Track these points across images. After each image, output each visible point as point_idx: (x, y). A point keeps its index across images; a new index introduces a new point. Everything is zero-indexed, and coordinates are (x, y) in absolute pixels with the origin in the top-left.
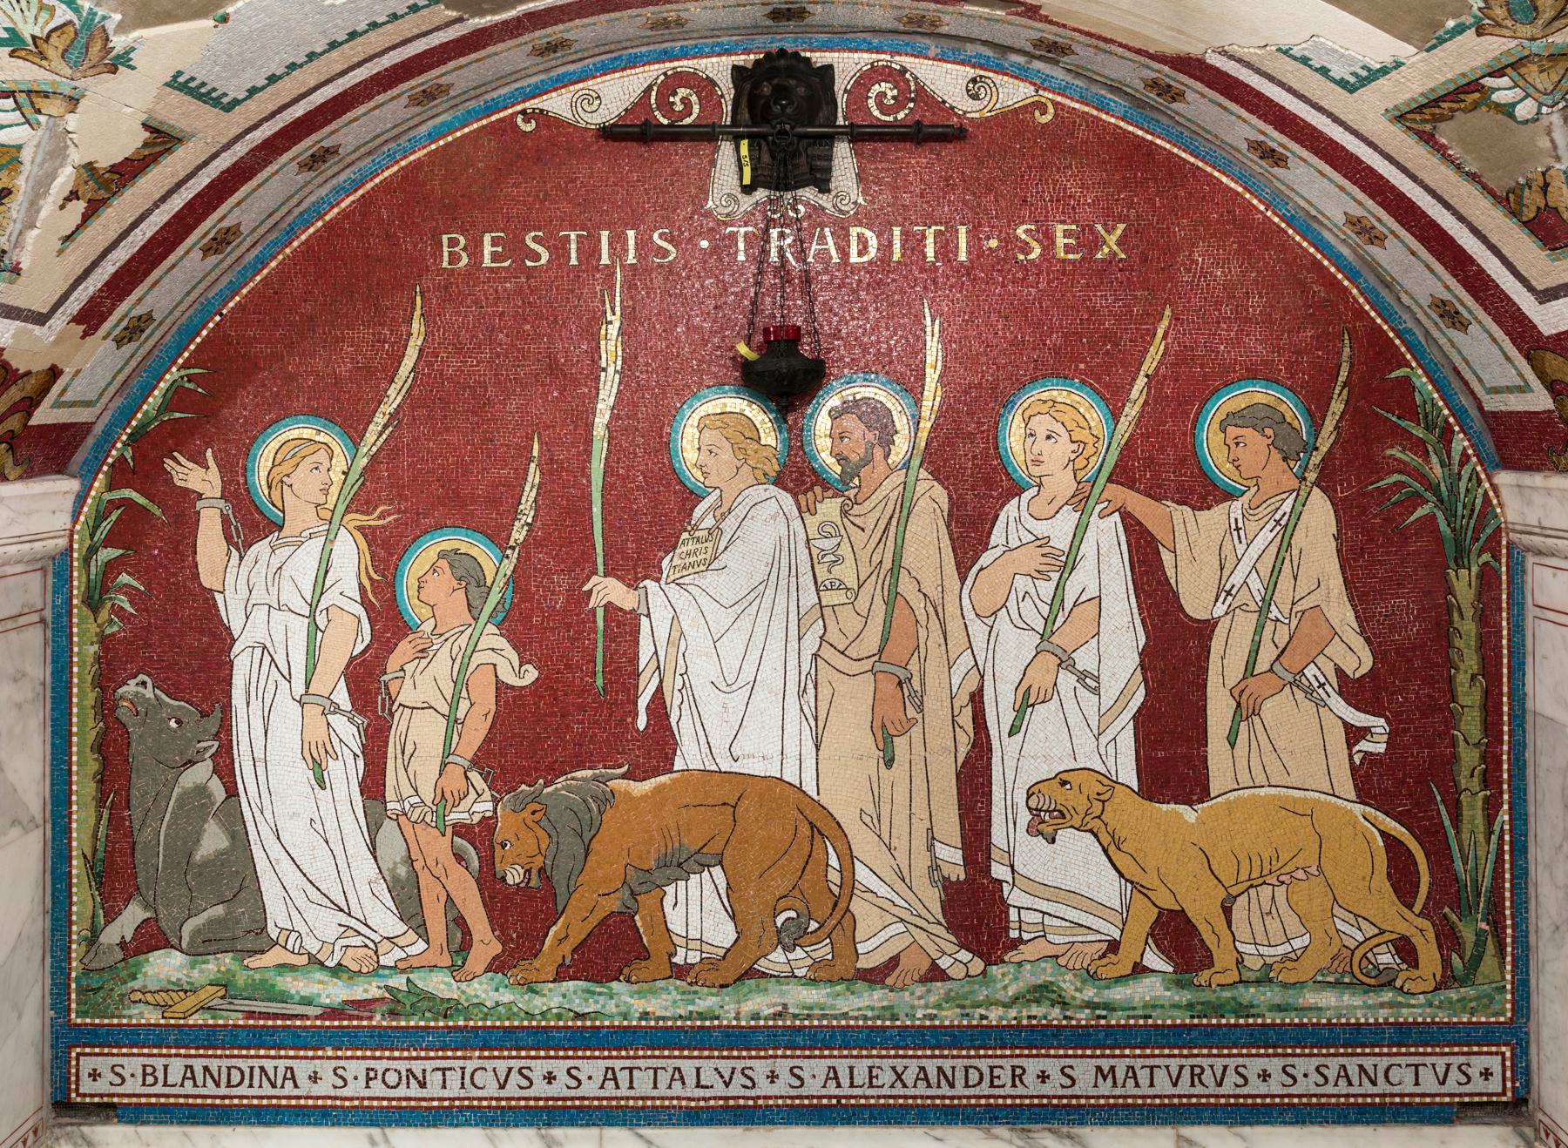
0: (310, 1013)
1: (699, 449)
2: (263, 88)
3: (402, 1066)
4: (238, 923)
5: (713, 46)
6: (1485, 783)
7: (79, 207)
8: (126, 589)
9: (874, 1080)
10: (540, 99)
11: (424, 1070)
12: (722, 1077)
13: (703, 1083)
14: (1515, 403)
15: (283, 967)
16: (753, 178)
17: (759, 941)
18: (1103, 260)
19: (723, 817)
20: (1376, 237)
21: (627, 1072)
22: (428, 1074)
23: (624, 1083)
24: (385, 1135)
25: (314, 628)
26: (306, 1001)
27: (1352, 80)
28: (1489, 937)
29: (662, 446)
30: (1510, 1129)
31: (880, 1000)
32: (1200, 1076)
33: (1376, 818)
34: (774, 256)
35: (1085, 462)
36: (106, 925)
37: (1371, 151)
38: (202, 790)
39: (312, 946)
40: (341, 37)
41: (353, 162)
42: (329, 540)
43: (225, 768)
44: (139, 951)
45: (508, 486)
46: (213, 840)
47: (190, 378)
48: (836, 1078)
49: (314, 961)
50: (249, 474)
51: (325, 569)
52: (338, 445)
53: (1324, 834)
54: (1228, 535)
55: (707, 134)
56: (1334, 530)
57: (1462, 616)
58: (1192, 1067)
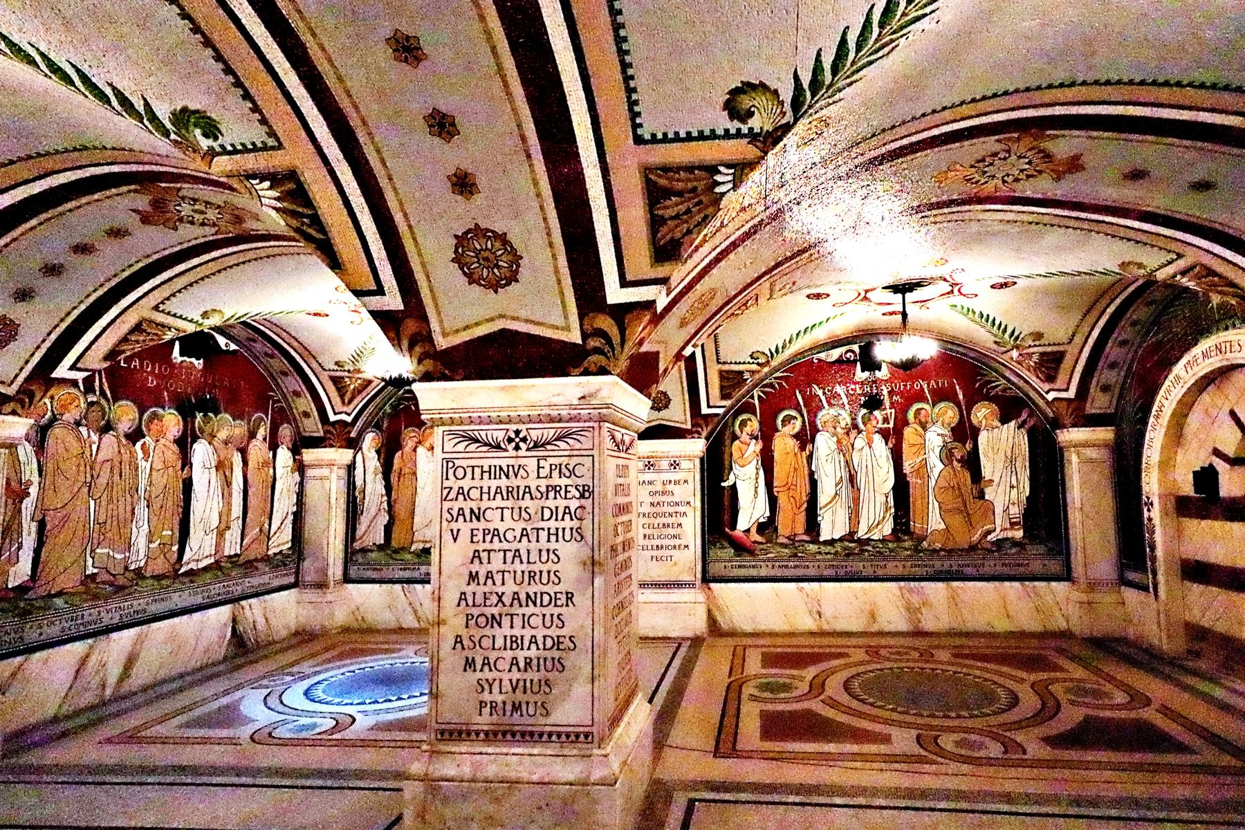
4: (623, 509)
7: (299, 638)
11: (520, 541)
13: (629, 277)
16: (657, 215)
19: (353, 572)
20: (961, 511)
21: (486, 553)
23: (499, 582)
30: (241, 708)
32: (571, 599)
34: (1062, 662)
35: (418, 694)
37: (606, 212)
44: (287, 179)
45: (408, 399)
52: (753, 418)
54: (568, 447)
58: (530, 572)
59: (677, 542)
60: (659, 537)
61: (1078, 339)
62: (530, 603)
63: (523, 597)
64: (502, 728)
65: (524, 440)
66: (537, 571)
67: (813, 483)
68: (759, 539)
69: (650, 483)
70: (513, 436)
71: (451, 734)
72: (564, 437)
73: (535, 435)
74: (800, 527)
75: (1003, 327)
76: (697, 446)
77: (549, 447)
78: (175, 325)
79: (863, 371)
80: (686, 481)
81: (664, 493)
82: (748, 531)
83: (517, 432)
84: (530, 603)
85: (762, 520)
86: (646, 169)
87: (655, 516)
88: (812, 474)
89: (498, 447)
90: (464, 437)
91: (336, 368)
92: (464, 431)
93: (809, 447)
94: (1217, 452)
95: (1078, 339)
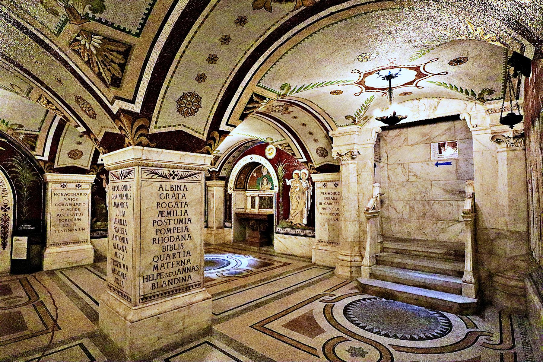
0: (248, 52)
1: (507, 164)
2: (270, 68)
5: (154, 286)
6: (532, 108)
12: (254, 325)
13: (229, 123)
14: (208, 176)
18: (485, 93)
24: (520, 113)
27: (503, 96)
29: (122, 52)
33: (234, 204)
36: (35, 144)
38: (103, 206)
40: (283, 57)
43: (105, 204)
46: (104, 211)
47: (257, 103)
55: (512, 111)
61: (45, 126)
62: (183, 239)
63: (180, 237)
64: (175, 289)
65: (176, 175)
66: (181, 227)
70: (172, 173)
71: (176, 291)
72: (194, 174)
73: (181, 173)
75: (126, 266)
76: (91, 178)
77: (186, 179)
78: (93, 75)
79: (289, 180)
83: (174, 172)
84: (183, 239)
86: (254, 93)
90: (151, 172)
92: (151, 169)
95: (45, 126)
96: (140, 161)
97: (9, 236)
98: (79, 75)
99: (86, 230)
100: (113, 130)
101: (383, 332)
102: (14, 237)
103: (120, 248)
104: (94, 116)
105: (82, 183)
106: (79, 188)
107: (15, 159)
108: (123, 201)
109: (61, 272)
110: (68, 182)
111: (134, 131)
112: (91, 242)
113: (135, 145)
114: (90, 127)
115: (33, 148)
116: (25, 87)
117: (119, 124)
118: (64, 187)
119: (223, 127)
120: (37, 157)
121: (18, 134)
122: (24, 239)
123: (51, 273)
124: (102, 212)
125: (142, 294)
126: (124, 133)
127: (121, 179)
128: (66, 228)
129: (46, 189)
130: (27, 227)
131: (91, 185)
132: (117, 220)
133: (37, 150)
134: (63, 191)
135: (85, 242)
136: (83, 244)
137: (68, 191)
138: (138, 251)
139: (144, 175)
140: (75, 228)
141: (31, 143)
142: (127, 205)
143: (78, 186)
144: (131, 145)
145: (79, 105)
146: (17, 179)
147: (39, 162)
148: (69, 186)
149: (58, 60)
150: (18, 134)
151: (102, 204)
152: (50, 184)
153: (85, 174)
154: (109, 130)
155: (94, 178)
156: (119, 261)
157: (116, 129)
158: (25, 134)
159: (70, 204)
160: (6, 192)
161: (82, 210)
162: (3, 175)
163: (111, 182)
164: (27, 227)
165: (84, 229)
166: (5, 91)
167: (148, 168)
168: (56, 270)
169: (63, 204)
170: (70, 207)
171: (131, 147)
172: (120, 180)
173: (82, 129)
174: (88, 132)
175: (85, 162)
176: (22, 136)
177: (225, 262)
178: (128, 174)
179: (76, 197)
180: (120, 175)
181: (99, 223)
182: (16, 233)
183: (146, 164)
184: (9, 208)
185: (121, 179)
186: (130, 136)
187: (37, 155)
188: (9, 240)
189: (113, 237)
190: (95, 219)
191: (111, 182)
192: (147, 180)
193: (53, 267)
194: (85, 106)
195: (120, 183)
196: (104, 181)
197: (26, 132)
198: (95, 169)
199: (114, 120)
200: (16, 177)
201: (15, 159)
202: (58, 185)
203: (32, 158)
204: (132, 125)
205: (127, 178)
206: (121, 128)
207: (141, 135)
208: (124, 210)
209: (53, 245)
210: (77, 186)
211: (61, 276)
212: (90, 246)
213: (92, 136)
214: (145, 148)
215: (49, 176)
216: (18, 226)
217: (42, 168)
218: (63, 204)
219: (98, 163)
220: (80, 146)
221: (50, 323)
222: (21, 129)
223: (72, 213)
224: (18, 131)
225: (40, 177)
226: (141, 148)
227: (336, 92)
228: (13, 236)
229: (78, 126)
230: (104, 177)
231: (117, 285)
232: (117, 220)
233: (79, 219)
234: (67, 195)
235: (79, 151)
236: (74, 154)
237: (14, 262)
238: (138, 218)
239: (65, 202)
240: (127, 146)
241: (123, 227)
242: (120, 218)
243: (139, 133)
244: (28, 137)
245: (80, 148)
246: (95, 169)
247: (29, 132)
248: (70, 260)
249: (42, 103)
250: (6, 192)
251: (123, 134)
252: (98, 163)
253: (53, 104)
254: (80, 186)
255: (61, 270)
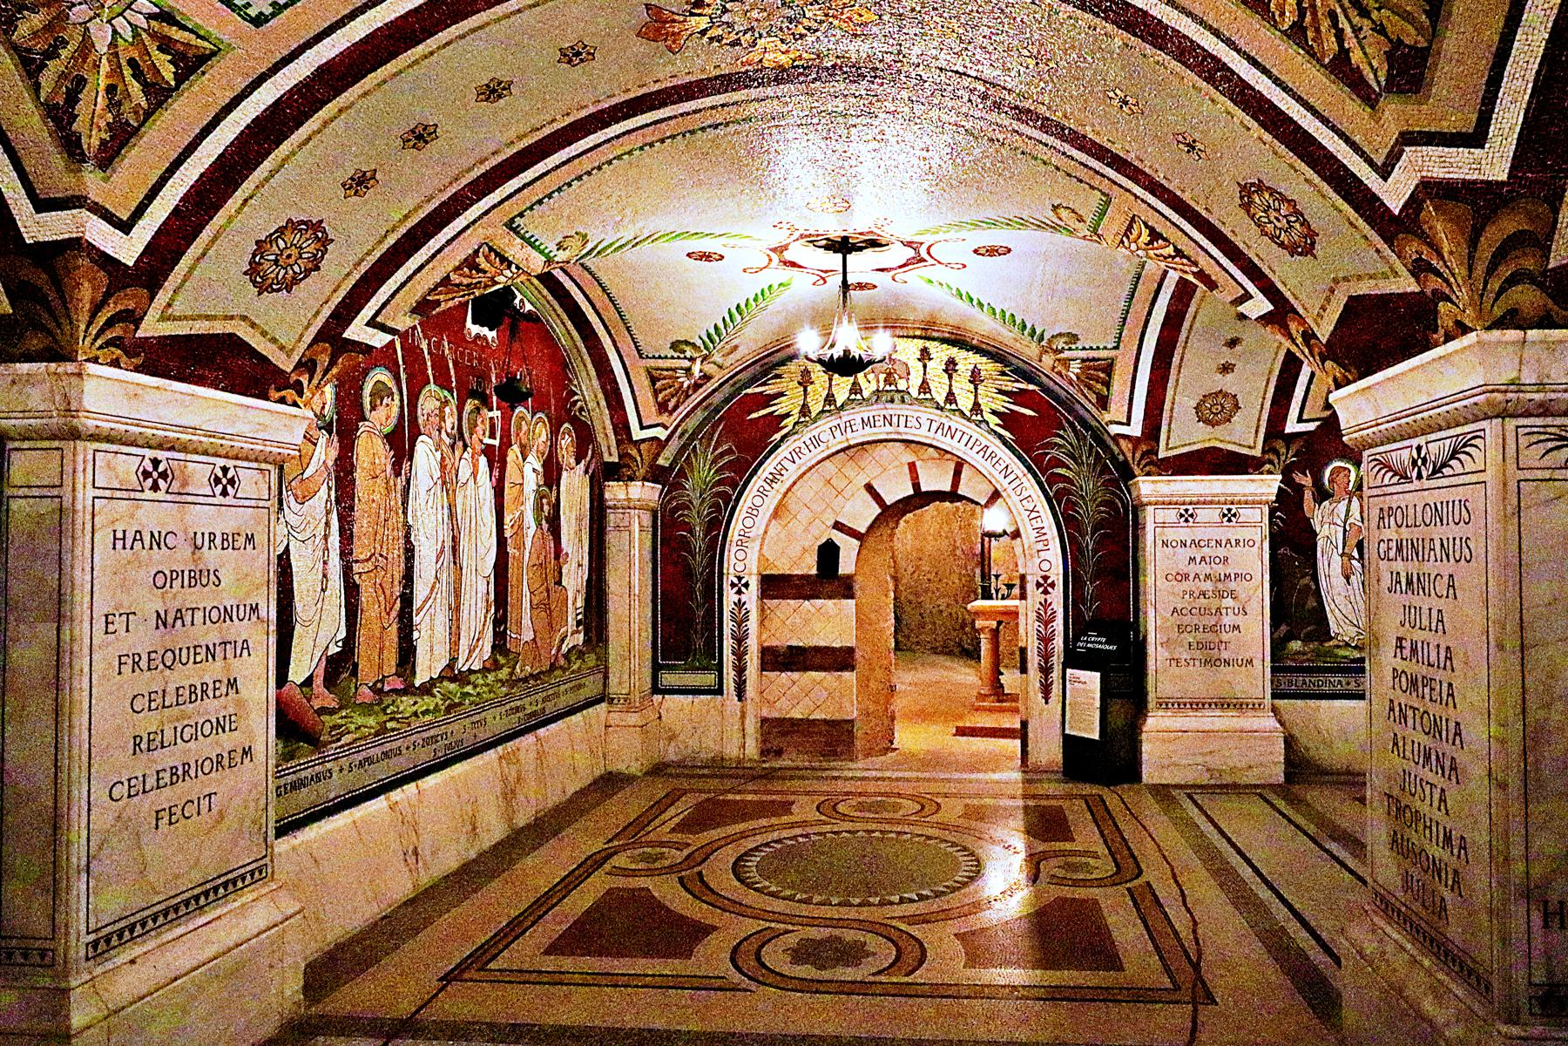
3: (734, 549)
8: (1279, 517)
9: (110, 626)
10: (463, 628)
15: (1338, 647)
17: (972, 134)
22: (1445, 594)
25: (1345, 531)
26: (1345, 657)
28: (104, 60)
31: (1303, 939)
35: (896, 898)
38: (1307, 586)
39: (1347, 639)
41: (309, 138)
42: (1350, 502)
43: (1315, 578)
46: (1312, 603)
48: (141, 540)
49: (1347, 645)
50: (67, 543)
51: (1348, 511)
53: (241, 311)
56: (416, 635)
57: (1373, 911)
59: (227, 741)
60: (179, 735)
67: (409, 552)
68: (331, 701)
69: (157, 541)
74: (390, 666)
75: (1008, 315)
76: (1268, 485)
80: (250, 539)
81: (197, 577)
82: (308, 682)
85: (333, 650)
87: (170, 658)
88: (408, 529)
89: (1404, 477)
91: (671, 353)
93: (406, 466)
94: (838, 526)
96: (1510, 395)
97: (1055, 666)
98: (1260, 97)
99: (1257, 663)
100: (1381, 283)
101: (835, 901)
102: (1069, 671)
103: (1427, 758)
104: (1305, 247)
105: (1239, 502)
106: (1229, 520)
107: (1058, 440)
108: (1430, 567)
109: (1190, 796)
110: (1198, 503)
111: (1480, 269)
112: (1274, 709)
113: (1489, 328)
114: (1288, 295)
115: (1103, 402)
116: (1089, 203)
117: (1412, 248)
118: (1187, 521)
119: (357, 331)
120: (1114, 429)
121: (1066, 363)
122: (1092, 679)
123: (1163, 792)
124: (1303, 606)
125: (1539, 977)
126: (1434, 283)
127: (1419, 477)
128: (1198, 654)
129: (1138, 526)
130: (1096, 642)
131: (1266, 510)
132: (1407, 644)
133: (1113, 407)
134: (1184, 534)
135: (1257, 707)
136: (1251, 713)
137: (1199, 534)
138: (1515, 783)
139: (1532, 456)
140: (1225, 655)
141: (1099, 386)
142: (1451, 586)
143: (1229, 516)
144: (1464, 329)
145: (1252, 216)
146: (1068, 500)
147: (1118, 444)
148: (1203, 514)
149: (1188, 67)
150: (1066, 363)
151: (1303, 577)
152: (1150, 509)
153: (1247, 473)
154: (1364, 288)
155: (1277, 484)
156: (1424, 808)
157: (1396, 274)
158: (1083, 361)
159: (1208, 577)
160: (1043, 538)
161: (1243, 596)
162: (1037, 487)
163: (1375, 492)
164: (1096, 642)
165: (1250, 662)
166: (1039, 233)
167: (1549, 420)
168: (1177, 786)
169: (1186, 577)
170: (1208, 586)
171: (1471, 338)
172: (1416, 484)
173: (1259, 305)
174: (1281, 314)
175: (1244, 434)
176: (1075, 367)
177: (872, 941)
178: (1452, 457)
179: (1221, 552)
180: (1414, 463)
181: (1296, 645)
182: (1074, 659)
183: (1541, 404)
184: (746, 585)
185: (1419, 477)
186: (1463, 295)
187: (1112, 422)
188: (1056, 675)
189: (1392, 709)
190: (1284, 628)
191: (1375, 492)
192: (1547, 474)
193: (1168, 778)
194: (1273, 214)
195: (1413, 497)
196: (1308, 495)
197: (1083, 354)
198: (1278, 455)
199: (1389, 240)
200: (1066, 492)
201: (1058, 440)
202: (1171, 515)
203: (1099, 435)
204: (1473, 243)
205: (1446, 471)
206: (1419, 269)
207: (1512, 281)
208: (1437, 604)
209: (1164, 704)
210: (1224, 515)
211: (1188, 804)
212: (1270, 722)
213: (1293, 326)
214: (1533, 334)
215: (1147, 487)
216: (1076, 639)
217: (1126, 460)
218: (1186, 577)
219: (1288, 430)
220: (1229, 376)
221: (1186, 976)
222: (1073, 347)
223: (1214, 603)
224: (1067, 354)
225: (1122, 492)
226: (1513, 335)
227: (706, 257)
228: (1065, 666)
229: (1247, 296)
230: (1306, 480)
231: (1417, 907)
232: (1407, 644)
233: (1236, 628)
234: (1197, 544)
235: (1226, 395)
236: (1216, 409)
237: (1071, 744)
238: (1512, 643)
239: (1193, 569)
240: (1449, 338)
241: (1439, 675)
242: (1419, 636)
243: (1505, 271)
244: (1089, 368)
245: (1228, 383)
246: (1278, 455)
247: (1092, 354)
248: (1215, 762)
249: (1133, 247)
250: (1043, 538)
251: (1428, 291)
252: (1288, 430)
253: (1165, 240)
254: (1234, 515)
255: (1191, 790)
